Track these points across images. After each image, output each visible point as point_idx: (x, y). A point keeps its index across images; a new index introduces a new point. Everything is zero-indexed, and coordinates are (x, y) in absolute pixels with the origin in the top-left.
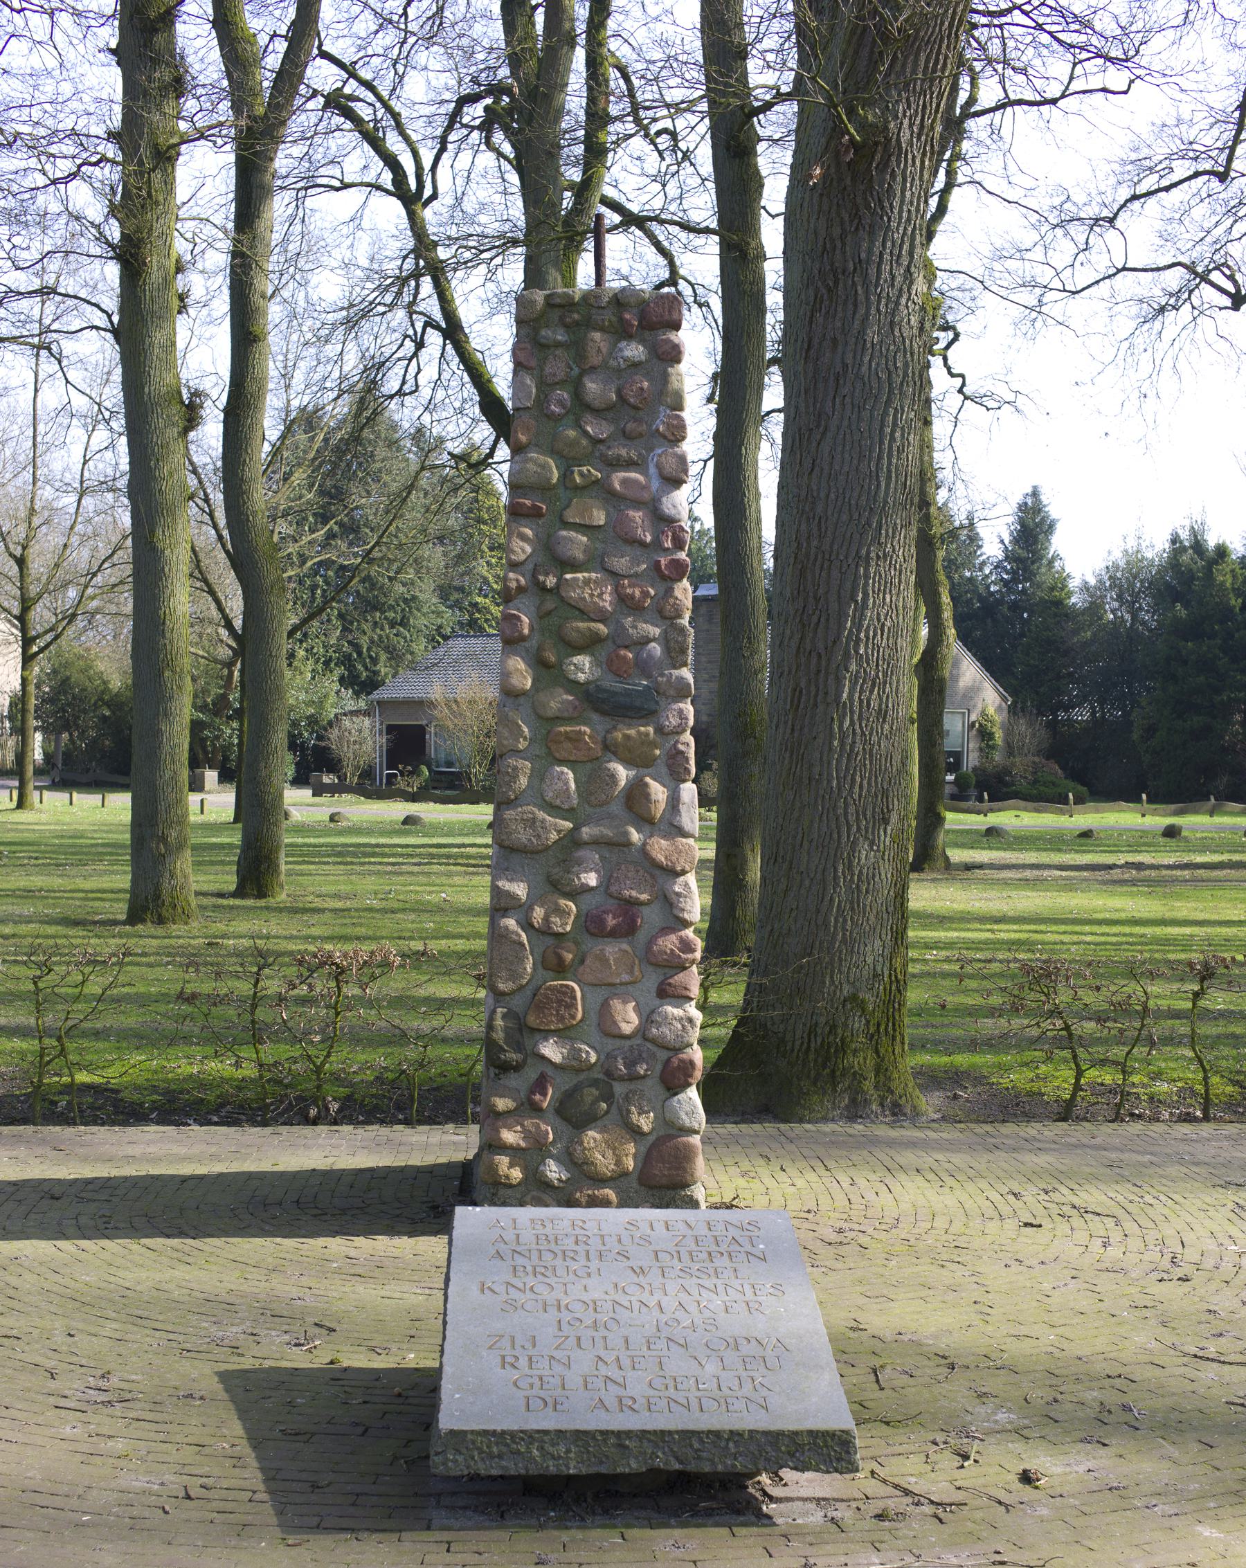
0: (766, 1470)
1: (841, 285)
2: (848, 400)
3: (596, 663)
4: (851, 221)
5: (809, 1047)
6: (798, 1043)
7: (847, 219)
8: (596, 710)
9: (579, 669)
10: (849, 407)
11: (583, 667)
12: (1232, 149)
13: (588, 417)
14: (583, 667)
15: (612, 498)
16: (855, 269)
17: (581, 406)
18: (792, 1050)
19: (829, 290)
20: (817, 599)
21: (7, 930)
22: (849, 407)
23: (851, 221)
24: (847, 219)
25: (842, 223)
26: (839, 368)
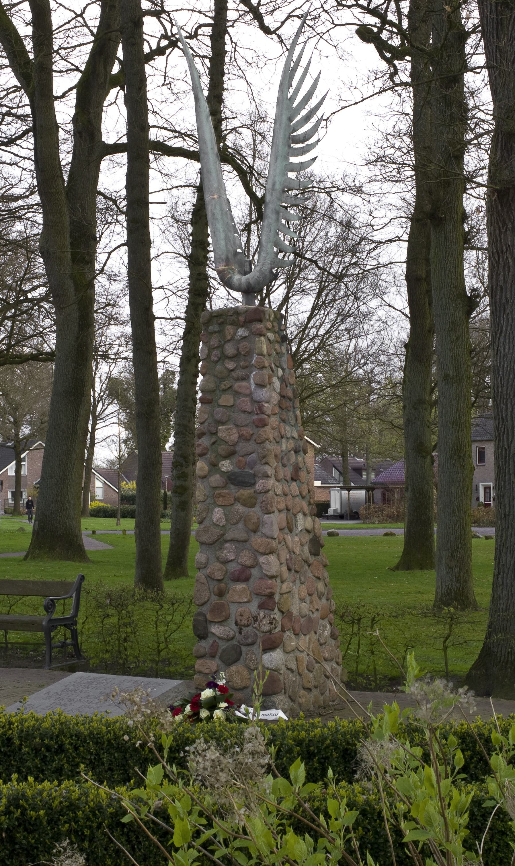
0: (88, 855)
1: (501, 259)
2: (510, 316)
3: (232, 463)
4: (503, 227)
5: (508, 661)
6: (503, 658)
7: (501, 226)
8: (232, 484)
9: (202, 469)
10: (510, 319)
11: (226, 465)
12: (173, 188)
13: (227, 361)
14: (226, 465)
15: (237, 394)
16: (507, 250)
17: (223, 357)
18: (500, 662)
19: (497, 262)
20: (503, 420)
21: (2, 556)
22: (510, 319)
23: (503, 227)
24: (501, 226)
25: (499, 228)
26: (504, 301)
